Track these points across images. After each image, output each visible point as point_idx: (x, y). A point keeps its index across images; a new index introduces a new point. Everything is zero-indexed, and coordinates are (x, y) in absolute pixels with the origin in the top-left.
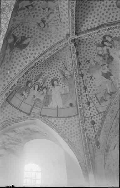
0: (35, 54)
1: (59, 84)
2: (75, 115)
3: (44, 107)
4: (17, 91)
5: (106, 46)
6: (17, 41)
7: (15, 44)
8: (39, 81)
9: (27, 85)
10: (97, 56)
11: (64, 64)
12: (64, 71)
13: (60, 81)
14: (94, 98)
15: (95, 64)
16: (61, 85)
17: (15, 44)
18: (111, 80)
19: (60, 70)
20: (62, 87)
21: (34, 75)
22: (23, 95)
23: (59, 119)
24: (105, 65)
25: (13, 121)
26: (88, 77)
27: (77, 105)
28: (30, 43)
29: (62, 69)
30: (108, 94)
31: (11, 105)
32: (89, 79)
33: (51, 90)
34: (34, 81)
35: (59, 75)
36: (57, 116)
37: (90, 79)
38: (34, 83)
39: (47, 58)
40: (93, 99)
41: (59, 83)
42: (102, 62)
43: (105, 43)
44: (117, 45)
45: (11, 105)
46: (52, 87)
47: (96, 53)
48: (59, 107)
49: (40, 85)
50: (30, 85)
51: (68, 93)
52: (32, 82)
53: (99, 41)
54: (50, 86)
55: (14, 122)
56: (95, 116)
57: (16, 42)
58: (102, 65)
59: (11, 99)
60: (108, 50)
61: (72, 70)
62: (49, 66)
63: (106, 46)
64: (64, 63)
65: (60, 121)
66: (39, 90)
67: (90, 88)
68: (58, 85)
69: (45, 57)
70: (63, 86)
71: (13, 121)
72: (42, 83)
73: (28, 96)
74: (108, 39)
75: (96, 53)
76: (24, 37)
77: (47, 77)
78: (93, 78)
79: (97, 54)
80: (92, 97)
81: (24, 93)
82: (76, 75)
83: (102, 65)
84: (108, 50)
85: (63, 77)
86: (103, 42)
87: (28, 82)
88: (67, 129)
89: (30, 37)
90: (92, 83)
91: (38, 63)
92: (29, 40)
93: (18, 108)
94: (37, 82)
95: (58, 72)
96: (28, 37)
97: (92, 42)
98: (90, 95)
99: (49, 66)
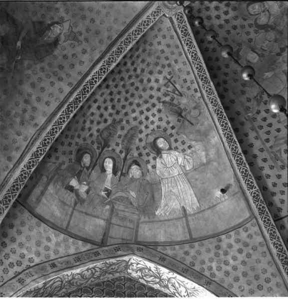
0: (81, 63)
1: (174, 145)
2: (246, 221)
3: (143, 219)
4: (51, 179)
6: (23, 34)
7: (19, 44)
8: (113, 145)
9: (79, 159)
10: (256, 32)
11: (169, 81)
12: (175, 102)
15: (258, 57)
16: (178, 144)
17: (19, 44)
18: (184, 6)
19: (164, 102)
21: (95, 128)
22: (71, 189)
23: (196, 244)
25: (53, 266)
26: (249, 100)
27: (241, 187)
28: (62, 37)
29: (168, 99)
31: (41, 219)
32: (255, 103)
33: (154, 167)
34: (98, 148)
35: (165, 119)
36: (188, 237)
37: (258, 105)
38: (100, 154)
39: (114, 65)
41: (172, 139)
42: (276, 44)
45: (41, 219)
46: (155, 159)
47: (250, 26)
48: (189, 210)
49: (119, 157)
50: (87, 159)
51: (205, 161)
52: (90, 150)
54: (148, 155)
55: (55, 269)
57: (21, 38)
58: (279, 51)
59: (39, 200)
61: (196, 91)
62: (131, 100)
64: (169, 77)
65: (203, 250)
66: (119, 173)
67: (266, 129)
68: (170, 149)
69: (109, 63)
70: (186, 146)
71: (53, 266)
72: (121, 152)
73: (87, 192)
76: (41, 23)
77: (132, 132)
80: (280, 150)
81: (74, 183)
82: (212, 96)
83: (279, 51)
87: (79, 150)
88: (229, 268)
89: (57, 23)
91: (91, 83)
92: (57, 29)
93: (64, 226)
94: (106, 149)
95: (159, 111)
96: (53, 24)
98: (271, 147)
99: (131, 100)
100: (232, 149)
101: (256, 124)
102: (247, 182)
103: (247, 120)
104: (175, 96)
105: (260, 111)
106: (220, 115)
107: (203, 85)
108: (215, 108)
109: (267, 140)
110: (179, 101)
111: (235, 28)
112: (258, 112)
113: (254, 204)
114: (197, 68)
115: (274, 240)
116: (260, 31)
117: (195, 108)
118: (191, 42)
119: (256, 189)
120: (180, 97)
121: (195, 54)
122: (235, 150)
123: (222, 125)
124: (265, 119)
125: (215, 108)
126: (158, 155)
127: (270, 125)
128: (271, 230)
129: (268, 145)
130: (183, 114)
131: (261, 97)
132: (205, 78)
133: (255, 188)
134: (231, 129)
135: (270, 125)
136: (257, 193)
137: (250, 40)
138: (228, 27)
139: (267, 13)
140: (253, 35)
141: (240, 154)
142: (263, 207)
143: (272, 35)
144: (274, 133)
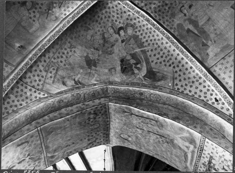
5: (120, 35)
13: (36, 8)
14: (54, 69)
20: (31, 18)
24: (98, 51)
30: (74, 80)
40: (51, 70)
43: (122, 33)
44: (130, 44)
47: (103, 31)
53: (120, 22)
56: (33, 90)
58: (96, 48)
60: (117, 41)
63: (120, 35)
68: (28, 10)
74: (130, 31)
75: (103, 31)
78: (73, 50)
79: (102, 33)
83: (96, 48)
84: (117, 41)
85: (45, 10)
86: (121, 28)
90: (68, 53)
97: (113, 16)
98: (52, 62)
100: (45, 44)
101: (60, 50)
102: (32, 57)
103: (60, 45)
104: (58, 4)
105: (66, 49)
106: (59, 31)
107: (70, 18)
108: (61, 28)
109: (54, 59)
110: (56, 7)
111: (100, 24)
112: (66, 49)
113: (23, 64)
114: (78, 12)
115: (11, 81)
116: (101, 36)
117: (56, 17)
118: (89, 5)
119: (31, 63)
120: (58, 7)
121: (84, 9)
122: (45, 45)
123: (55, 34)
124: (64, 53)
125: (61, 28)
126: (22, 4)
127: (62, 57)
128: (15, 78)
129: (53, 60)
130: (50, 11)
131: (73, 47)
132: (74, 18)
133: (31, 62)
134: (55, 39)
135: (62, 57)
136: (29, 64)
137: (96, 33)
138: (99, 19)
139: (110, 36)
140: (99, 33)
141: (44, 48)
142: (24, 70)
143: (101, 42)
144: (59, 60)
